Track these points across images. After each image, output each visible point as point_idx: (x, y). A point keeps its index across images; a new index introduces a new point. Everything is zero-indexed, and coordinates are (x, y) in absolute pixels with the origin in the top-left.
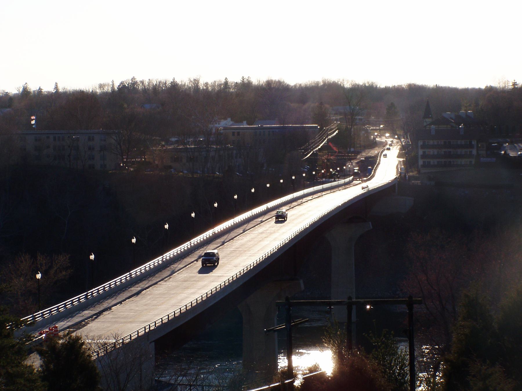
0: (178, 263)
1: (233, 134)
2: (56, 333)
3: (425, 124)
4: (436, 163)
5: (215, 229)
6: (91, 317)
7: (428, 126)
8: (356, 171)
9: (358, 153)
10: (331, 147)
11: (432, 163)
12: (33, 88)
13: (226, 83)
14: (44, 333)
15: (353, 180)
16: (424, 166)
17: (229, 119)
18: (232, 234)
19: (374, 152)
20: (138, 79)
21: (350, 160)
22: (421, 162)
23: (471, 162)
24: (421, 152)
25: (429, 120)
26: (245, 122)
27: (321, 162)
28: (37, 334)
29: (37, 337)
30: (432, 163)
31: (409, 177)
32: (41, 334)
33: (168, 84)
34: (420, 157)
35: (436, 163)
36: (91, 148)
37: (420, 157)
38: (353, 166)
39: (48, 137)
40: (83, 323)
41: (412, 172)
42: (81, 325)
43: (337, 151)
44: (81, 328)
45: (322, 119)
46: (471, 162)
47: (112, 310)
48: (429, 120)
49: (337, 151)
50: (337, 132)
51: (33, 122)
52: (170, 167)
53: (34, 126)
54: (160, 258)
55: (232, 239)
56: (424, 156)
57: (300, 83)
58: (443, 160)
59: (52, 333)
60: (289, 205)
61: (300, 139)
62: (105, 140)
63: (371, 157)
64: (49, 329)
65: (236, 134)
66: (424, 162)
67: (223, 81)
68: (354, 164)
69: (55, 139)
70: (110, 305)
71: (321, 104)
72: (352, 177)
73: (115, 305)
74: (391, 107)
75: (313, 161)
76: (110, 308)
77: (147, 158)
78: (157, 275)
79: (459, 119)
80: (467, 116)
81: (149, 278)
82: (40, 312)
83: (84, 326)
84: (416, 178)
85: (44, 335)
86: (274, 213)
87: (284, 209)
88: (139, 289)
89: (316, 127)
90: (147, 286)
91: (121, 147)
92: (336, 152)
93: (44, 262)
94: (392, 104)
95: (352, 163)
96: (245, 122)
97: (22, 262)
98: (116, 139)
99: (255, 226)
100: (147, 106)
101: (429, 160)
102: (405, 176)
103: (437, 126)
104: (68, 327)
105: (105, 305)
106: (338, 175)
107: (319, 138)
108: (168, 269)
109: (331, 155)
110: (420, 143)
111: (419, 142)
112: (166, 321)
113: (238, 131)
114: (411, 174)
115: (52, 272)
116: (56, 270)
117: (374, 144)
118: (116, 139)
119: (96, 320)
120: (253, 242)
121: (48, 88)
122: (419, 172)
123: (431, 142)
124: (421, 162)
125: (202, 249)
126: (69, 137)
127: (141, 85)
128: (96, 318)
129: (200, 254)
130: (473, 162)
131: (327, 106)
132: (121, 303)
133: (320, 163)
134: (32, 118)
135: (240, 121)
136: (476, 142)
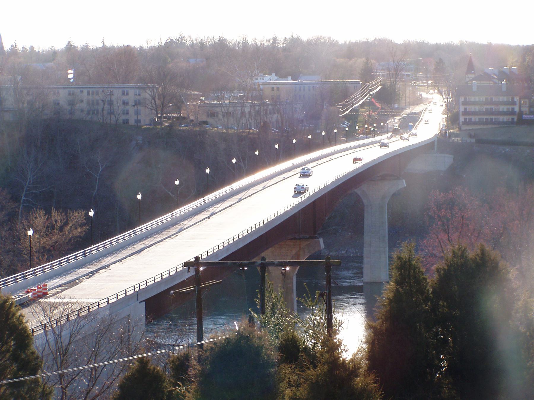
0: (188, 220)
1: (273, 89)
2: (45, 291)
3: (468, 80)
4: (477, 120)
5: (232, 185)
6: (87, 275)
7: (470, 82)
8: (396, 127)
9: (403, 109)
10: (374, 103)
11: (473, 120)
12: (79, 44)
13: (275, 39)
14: (31, 291)
15: (391, 136)
16: (465, 122)
17: (274, 74)
18: (251, 191)
19: (417, 109)
20: (186, 35)
21: (394, 116)
22: (462, 119)
23: (513, 119)
24: (462, 109)
25: (472, 76)
26: (290, 78)
27: (362, 118)
28: (24, 293)
29: (22, 296)
30: (473, 120)
31: (450, 134)
32: (28, 292)
33: (217, 39)
34: (461, 113)
35: (477, 120)
36: (125, 103)
37: (461, 113)
38: (394, 122)
39: (82, 92)
40: (77, 281)
41: (453, 129)
42: (74, 283)
43: (380, 107)
44: (73, 286)
45: (367, 74)
46: (513, 119)
47: (109, 268)
48: (472, 76)
49: (380, 107)
50: (380, 88)
51: (70, 76)
52: (206, 123)
53: (72, 80)
54: (169, 215)
55: (250, 196)
56: (465, 113)
57: (211, 36)
58: (485, 117)
59: (41, 292)
60: (317, 162)
61: (342, 94)
62: (139, 95)
63: (415, 113)
64: (38, 287)
65: (275, 88)
66: (465, 119)
67: (271, 37)
68: (396, 121)
69: (88, 94)
70: (109, 263)
71: (368, 59)
72: (391, 134)
73: (115, 263)
74: (440, 65)
75: (352, 118)
76: (108, 266)
77: (183, 113)
78: (164, 232)
79: (502, 75)
80: (511, 72)
81: (155, 235)
82: (32, 269)
83: (78, 284)
84: (456, 135)
85: (31, 294)
86: (299, 170)
87: (309, 166)
88: (143, 246)
89: (358, 83)
90: (151, 243)
91: (155, 102)
92: (378, 108)
93: (59, 218)
94: (440, 59)
95: (394, 119)
96: (290, 78)
97: (36, 218)
98: (150, 93)
99: (276, 183)
100: (192, 61)
101: (470, 117)
102: (446, 133)
103: (479, 82)
104: (60, 286)
105: (104, 262)
106: (376, 131)
107: (362, 93)
108: (177, 226)
109: (373, 112)
110: (462, 99)
111: (460, 98)
112: (160, 279)
113: (278, 86)
114: (452, 131)
115: (67, 229)
116: (71, 227)
117: (419, 101)
118: (150, 93)
119: (91, 278)
120: (262, 200)
121: (95, 43)
122: (460, 129)
123: (501, 99)
124: (462, 119)
125: (217, 206)
126: (103, 91)
127: (189, 39)
128: (92, 276)
129: (213, 211)
130: (515, 120)
131: (373, 61)
132: (120, 261)
133: (360, 119)
134: (70, 71)
135: (285, 77)
136: (518, 99)
